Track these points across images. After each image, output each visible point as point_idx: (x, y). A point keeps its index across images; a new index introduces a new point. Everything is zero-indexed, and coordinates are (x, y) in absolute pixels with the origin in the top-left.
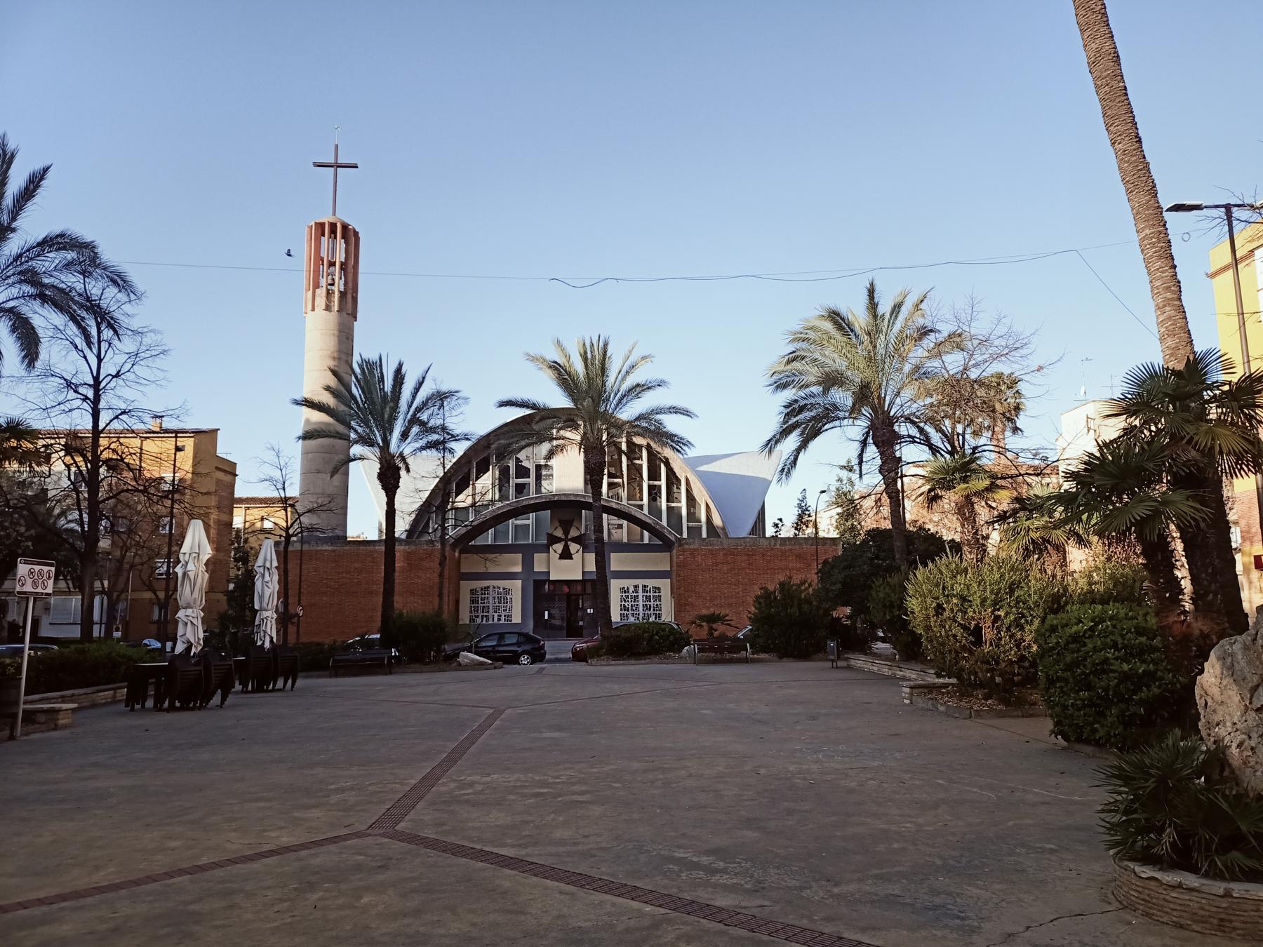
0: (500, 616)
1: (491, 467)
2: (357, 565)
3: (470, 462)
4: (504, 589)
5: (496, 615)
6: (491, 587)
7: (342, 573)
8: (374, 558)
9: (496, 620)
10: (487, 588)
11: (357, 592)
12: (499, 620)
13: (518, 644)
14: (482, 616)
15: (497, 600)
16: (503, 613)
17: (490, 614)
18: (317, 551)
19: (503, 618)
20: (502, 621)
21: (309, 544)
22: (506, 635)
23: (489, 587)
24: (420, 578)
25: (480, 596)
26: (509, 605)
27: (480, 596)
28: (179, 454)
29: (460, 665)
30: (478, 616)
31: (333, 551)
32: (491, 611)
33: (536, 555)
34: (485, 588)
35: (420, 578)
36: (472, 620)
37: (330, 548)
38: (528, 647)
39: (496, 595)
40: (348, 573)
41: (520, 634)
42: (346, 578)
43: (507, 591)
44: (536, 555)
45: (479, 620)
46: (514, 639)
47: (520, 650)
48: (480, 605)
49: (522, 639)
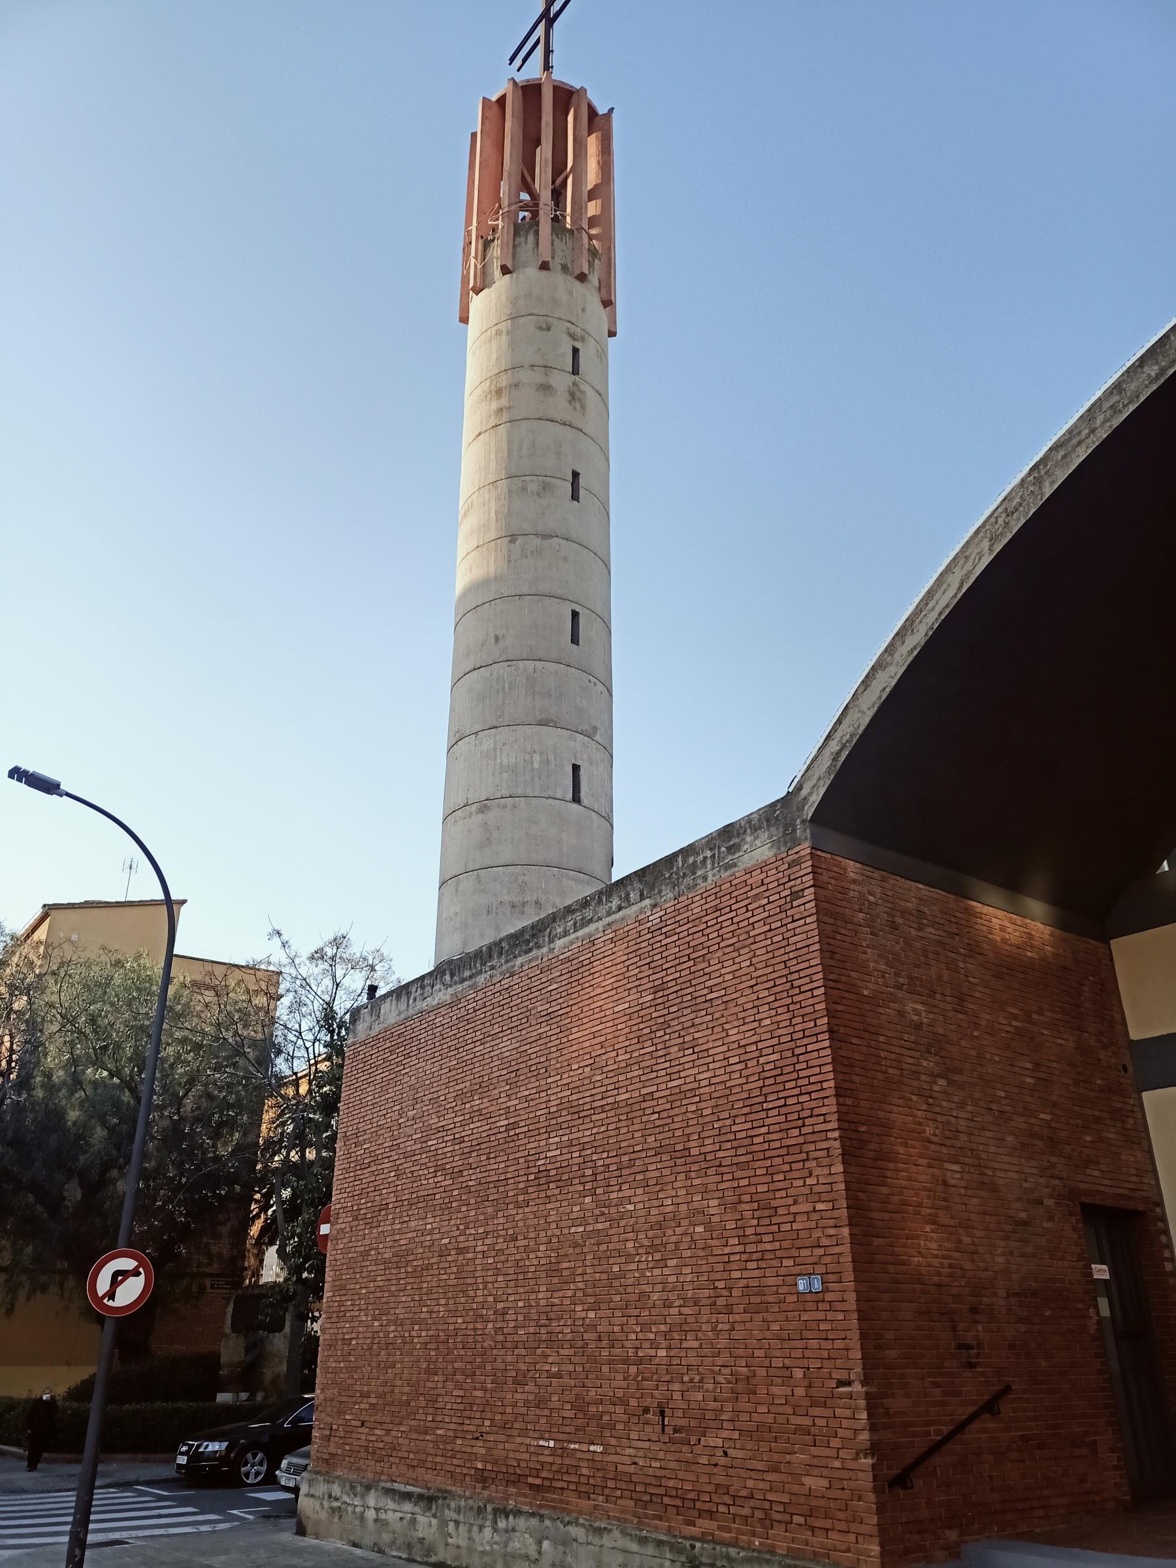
31: (455, 1003)
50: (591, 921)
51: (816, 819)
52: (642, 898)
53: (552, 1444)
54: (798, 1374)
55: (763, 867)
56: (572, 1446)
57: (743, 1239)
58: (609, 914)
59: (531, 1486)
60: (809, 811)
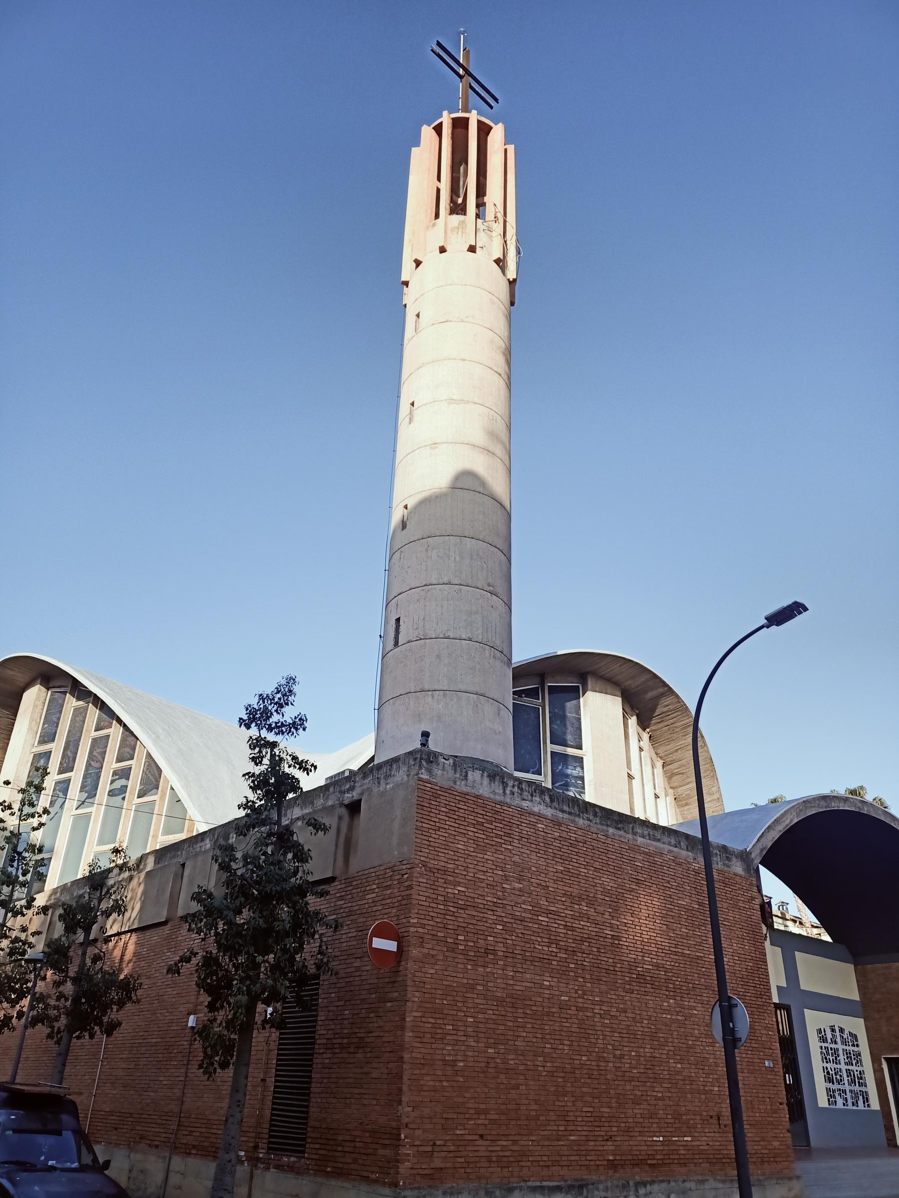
18: (522, 812)
37: (549, 812)
50: (659, 840)
53: (661, 1139)
56: (674, 1139)
59: (650, 1165)
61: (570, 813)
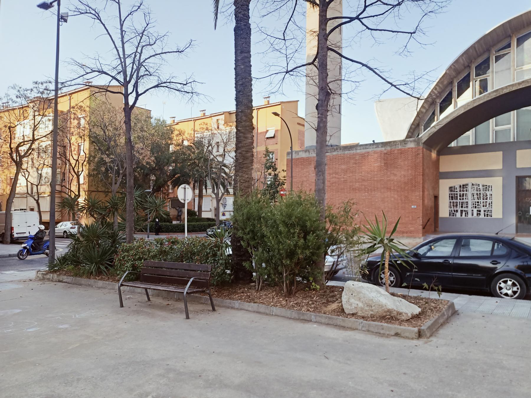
0: (480, 211)
1: (471, 83)
2: (343, 167)
3: (451, 83)
4: (483, 186)
5: (475, 211)
6: (470, 185)
7: (333, 173)
8: (356, 160)
9: (475, 214)
10: (464, 186)
11: (344, 189)
12: (478, 214)
13: (493, 258)
14: (462, 211)
15: (476, 196)
16: (482, 209)
17: (469, 209)
19: (482, 213)
20: (482, 216)
21: (309, 152)
22: (472, 241)
23: (467, 185)
24: (395, 175)
25: (458, 193)
26: (488, 201)
27: (458, 193)
28: (63, 25)
29: (341, 311)
30: (457, 211)
32: (470, 205)
33: (518, 152)
34: (463, 186)
35: (395, 175)
36: (452, 214)
38: (512, 265)
39: (475, 192)
40: (336, 173)
41: (495, 240)
42: (335, 177)
43: (487, 188)
44: (518, 152)
45: (458, 215)
46: (485, 247)
47: (500, 267)
48: (458, 201)
49: (500, 250)
50: (368, 148)
51: (425, 143)
52: (382, 147)
54: (411, 217)
55: (412, 148)
57: (402, 201)
58: (373, 148)
60: (423, 141)
61: (331, 152)
